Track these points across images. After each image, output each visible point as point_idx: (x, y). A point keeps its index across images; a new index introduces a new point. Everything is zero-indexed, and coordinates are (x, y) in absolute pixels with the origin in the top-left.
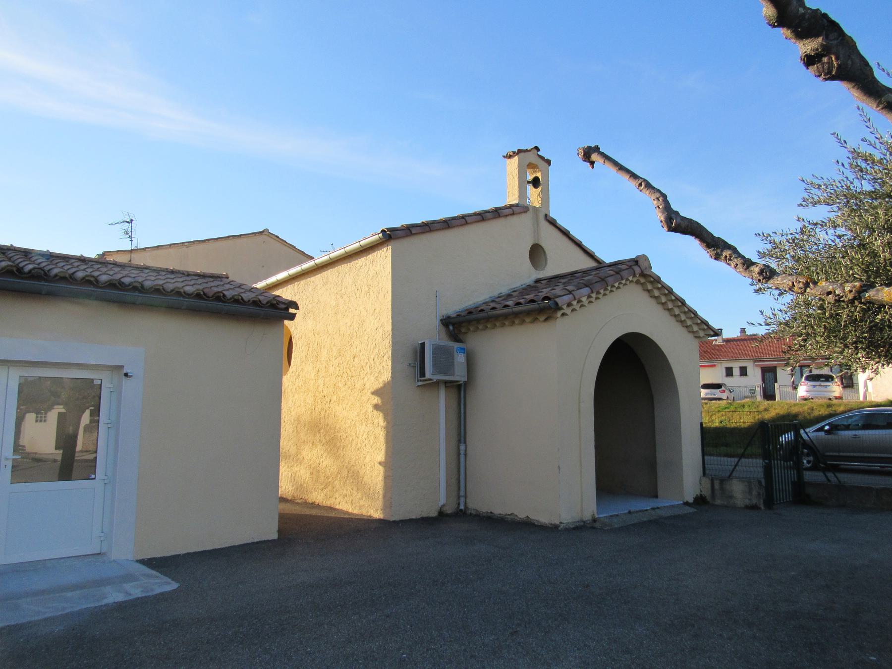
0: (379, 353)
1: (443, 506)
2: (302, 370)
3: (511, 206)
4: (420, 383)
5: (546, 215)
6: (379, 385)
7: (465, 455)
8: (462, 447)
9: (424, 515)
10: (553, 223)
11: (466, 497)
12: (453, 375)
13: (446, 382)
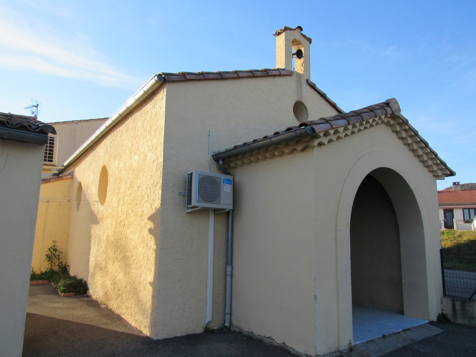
0: (154, 183)
1: (209, 323)
2: (112, 200)
3: (278, 70)
4: (189, 210)
5: (307, 80)
6: (152, 212)
7: (232, 275)
8: (229, 269)
9: (190, 332)
10: (313, 86)
11: (231, 314)
12: (219, 203)
13: (215, 210)
